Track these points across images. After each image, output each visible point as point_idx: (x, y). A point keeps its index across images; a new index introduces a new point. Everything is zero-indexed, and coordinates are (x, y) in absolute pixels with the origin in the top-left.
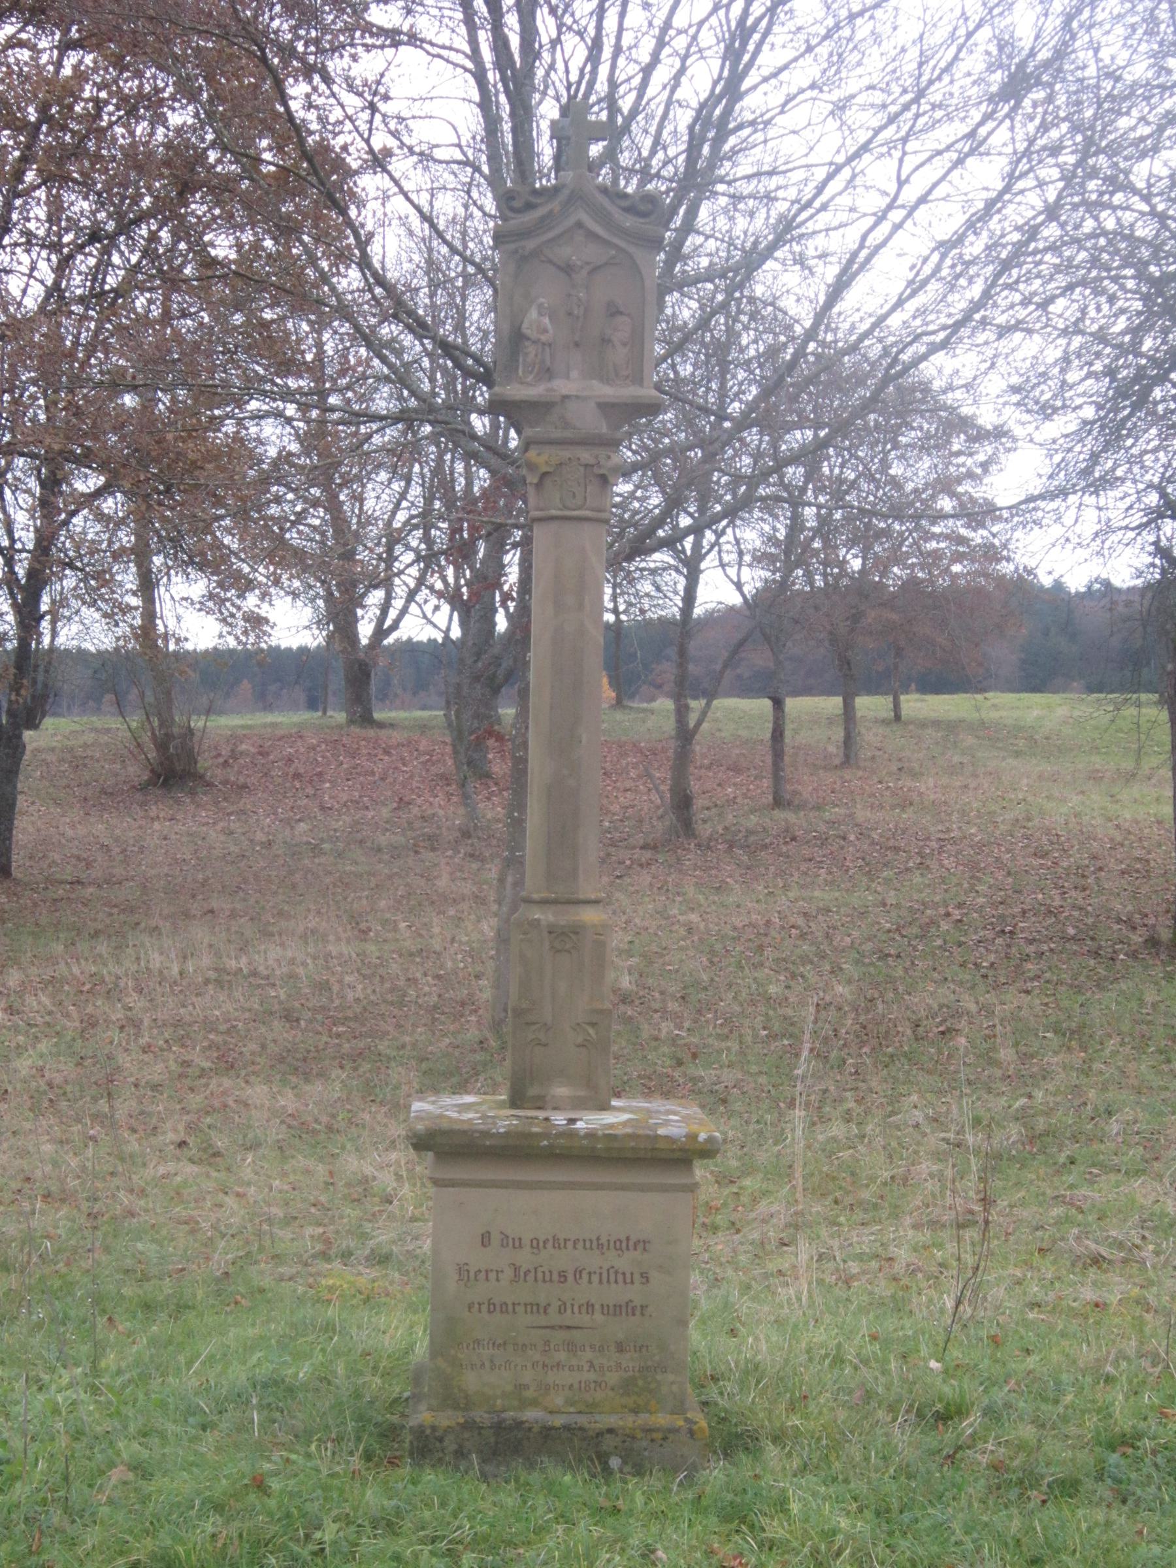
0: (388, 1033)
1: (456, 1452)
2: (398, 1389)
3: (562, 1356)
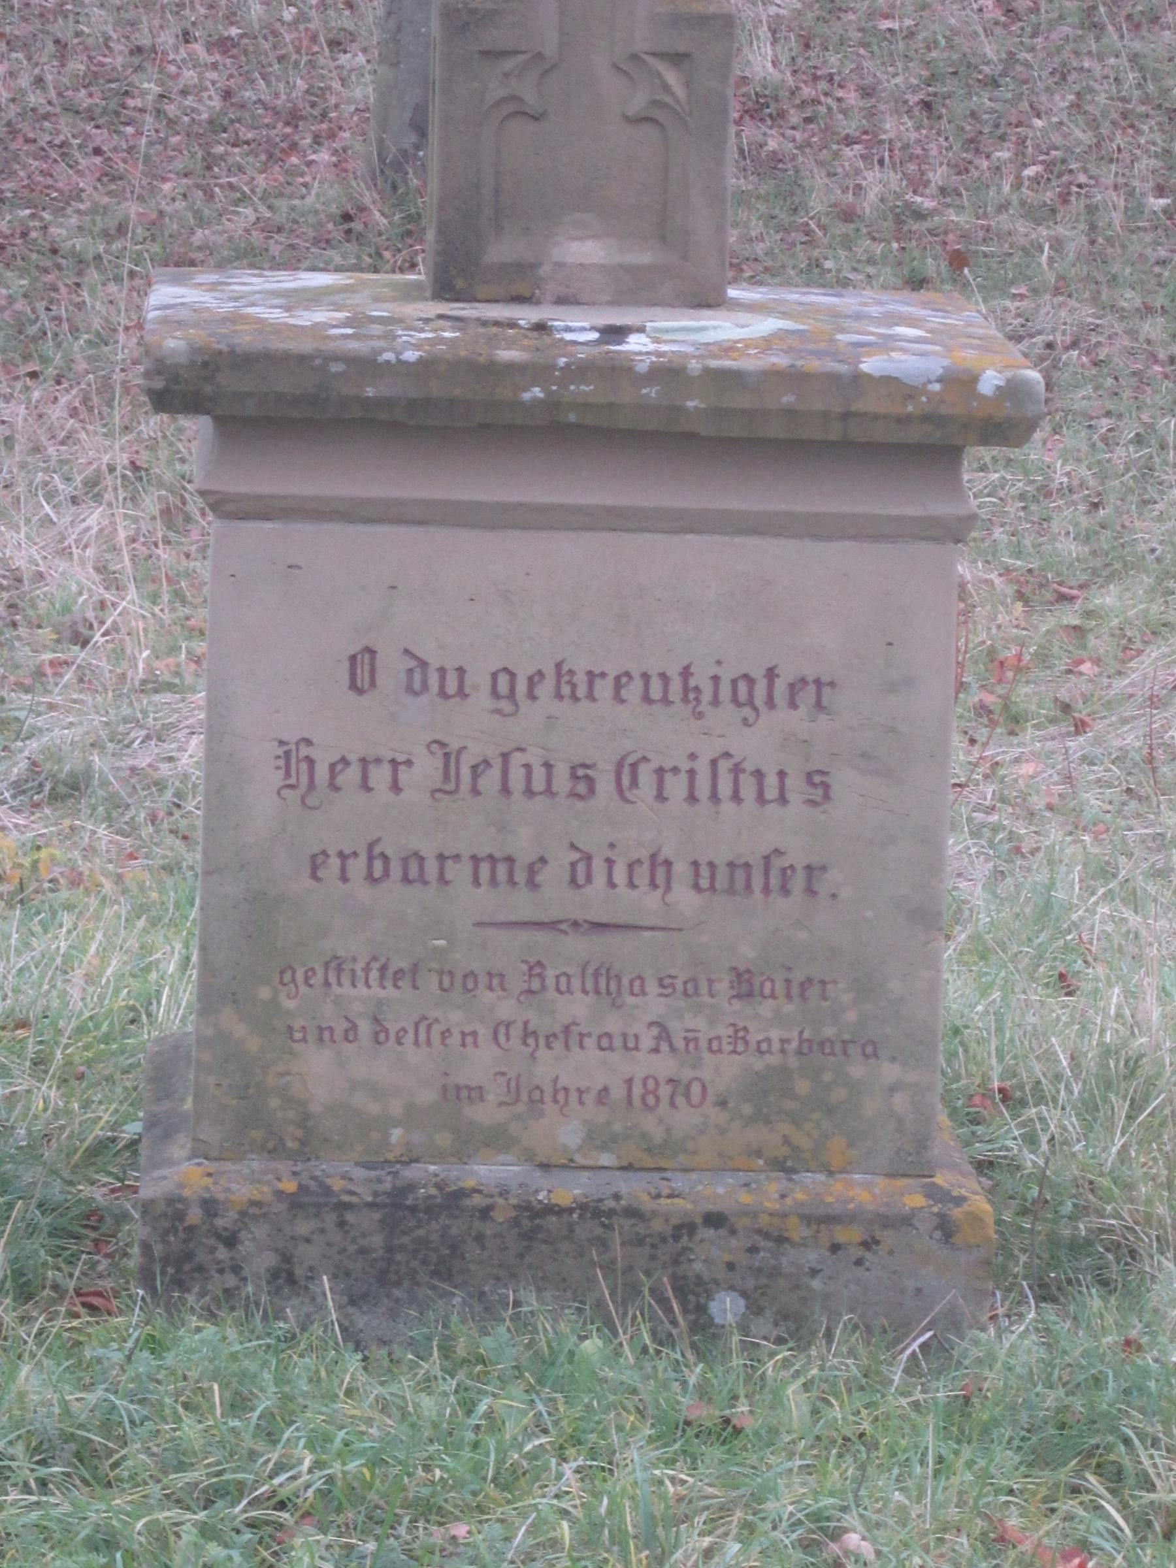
0: (78, 195)
1: (274, 1274)
2: (104, 1115)
3: (577, 1007)
